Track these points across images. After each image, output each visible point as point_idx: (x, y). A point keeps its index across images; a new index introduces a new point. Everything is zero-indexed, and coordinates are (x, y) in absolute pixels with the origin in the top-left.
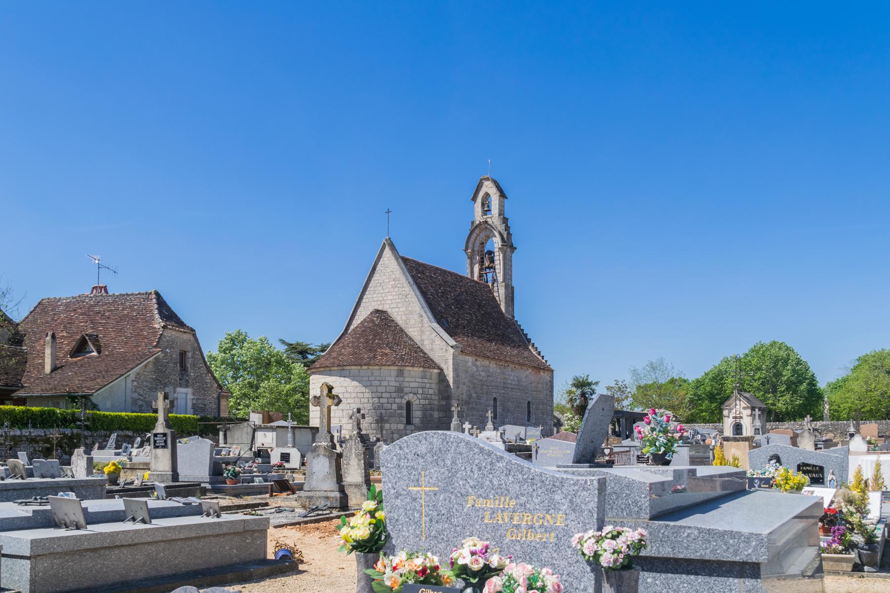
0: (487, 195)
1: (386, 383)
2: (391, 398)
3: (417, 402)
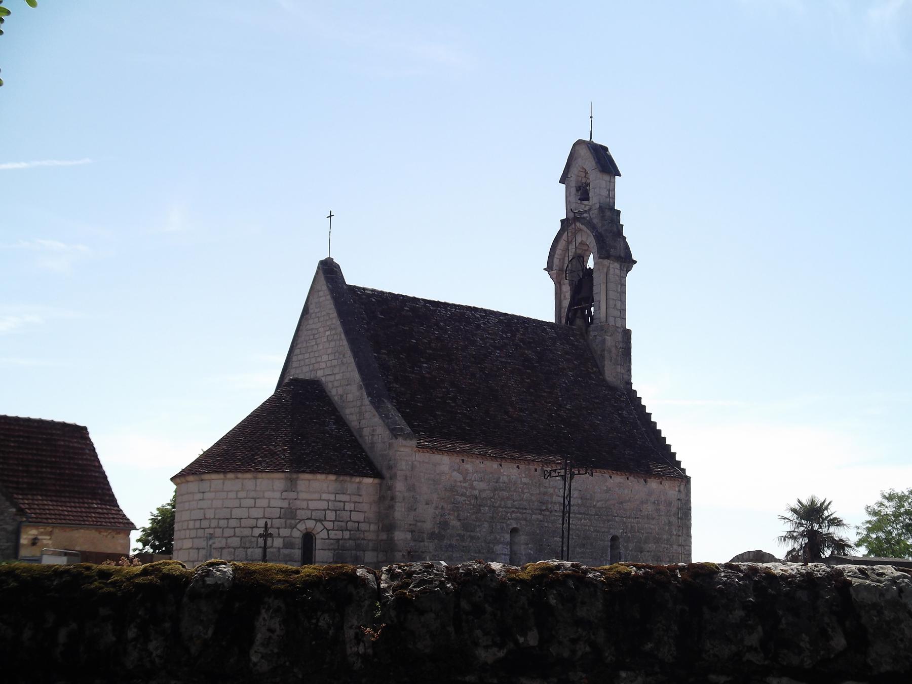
1: (264, 503)
3: (324, 534)
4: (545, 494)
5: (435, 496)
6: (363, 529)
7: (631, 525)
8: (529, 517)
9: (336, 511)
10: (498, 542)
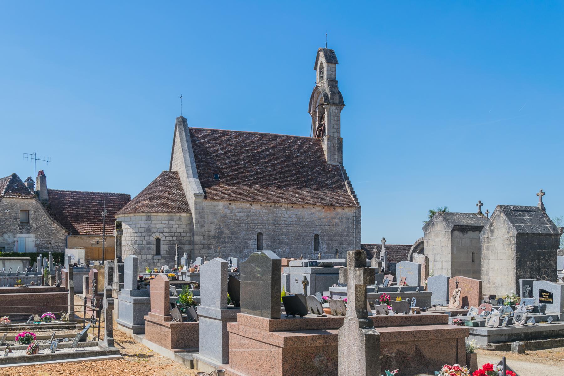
0: (322, 63)
1: (138, 226)
2: (142, 236)
3: (164, 238)
4: (276, 217)
5: (215, 220)
6: (183, 235)
7: (326, 229)
8: (267, 227)
9: (169, 228)
10: (251, 239)
